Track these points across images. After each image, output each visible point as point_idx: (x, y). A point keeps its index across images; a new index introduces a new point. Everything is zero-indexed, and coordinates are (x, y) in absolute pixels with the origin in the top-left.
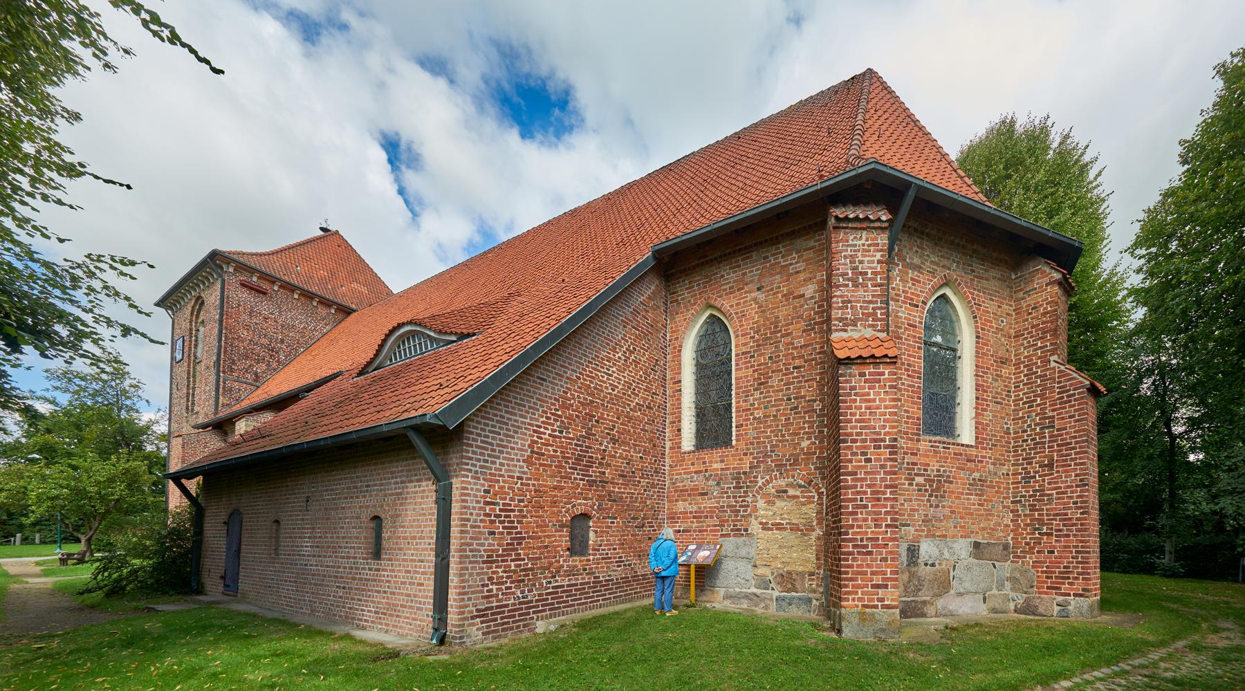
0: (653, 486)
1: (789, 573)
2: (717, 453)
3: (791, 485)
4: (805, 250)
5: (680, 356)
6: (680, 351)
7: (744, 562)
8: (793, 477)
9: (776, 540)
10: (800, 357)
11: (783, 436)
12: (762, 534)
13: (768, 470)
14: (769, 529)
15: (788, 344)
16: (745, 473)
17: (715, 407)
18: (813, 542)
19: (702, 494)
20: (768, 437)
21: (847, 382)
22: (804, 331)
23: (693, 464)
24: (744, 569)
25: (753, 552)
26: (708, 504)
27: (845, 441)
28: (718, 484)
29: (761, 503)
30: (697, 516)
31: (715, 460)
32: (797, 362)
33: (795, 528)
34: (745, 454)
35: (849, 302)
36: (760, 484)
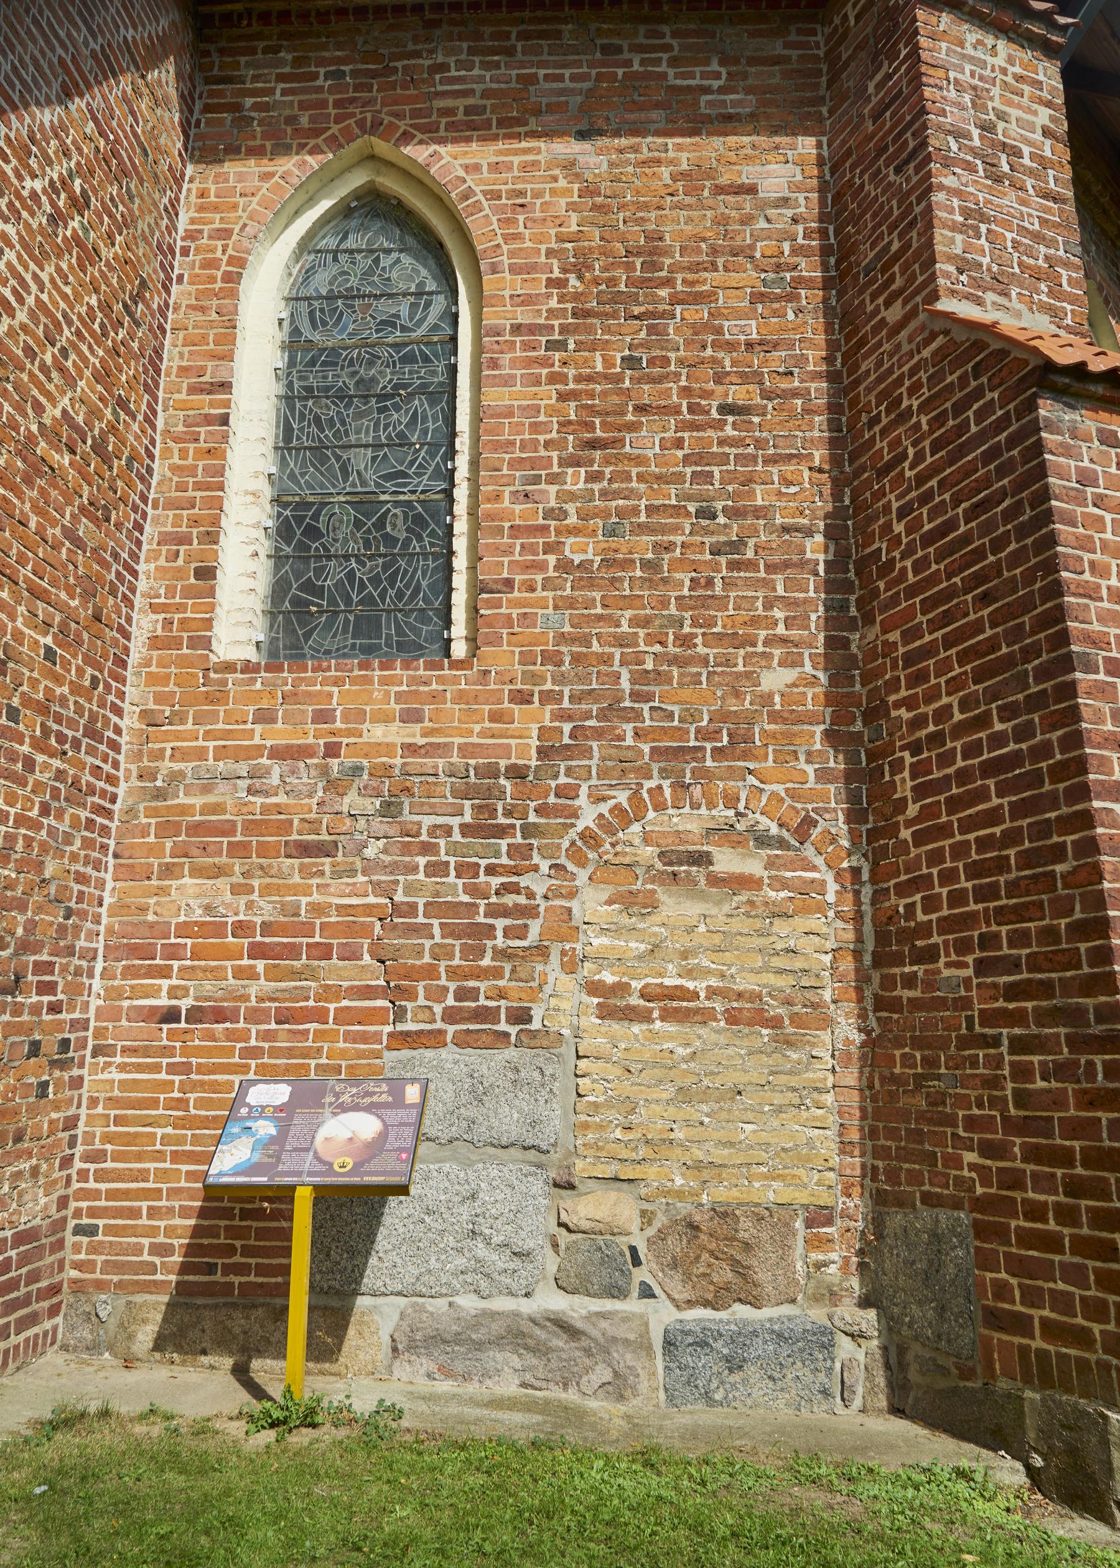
0: (78, 792)
1: (723, 1213)
2: (388, 684)
3: (724, 833)
4: (753, 61)
5: (234, 294)
6: (234, 279)
7: (513, 1166)
8: (731, 801)
9: (666, 1064)
10: (745, 378)
11: (686, 641)
12: (598, 1034)
13: (624, 767)
14: (630, 1015)
15: (697, 329)
16: (517, 773)
17: (365, 505)
18: (820, 1074)
19: (305, 850)
20: (621, 641)
21: (1067, 451)
22: (758, 298)
23: (265, 717)
24: (515, 1200)
25: (555, 1122)
26: (332, 892)
27: (1090, 667)
28: (389, 809)
29: (592, 903)
30: (273, 947)
31: (376, 709)
32: (736, 394)
33: (746, 1013)
34: (522, 698)
35: (984, 218)
36: (587, 820)
